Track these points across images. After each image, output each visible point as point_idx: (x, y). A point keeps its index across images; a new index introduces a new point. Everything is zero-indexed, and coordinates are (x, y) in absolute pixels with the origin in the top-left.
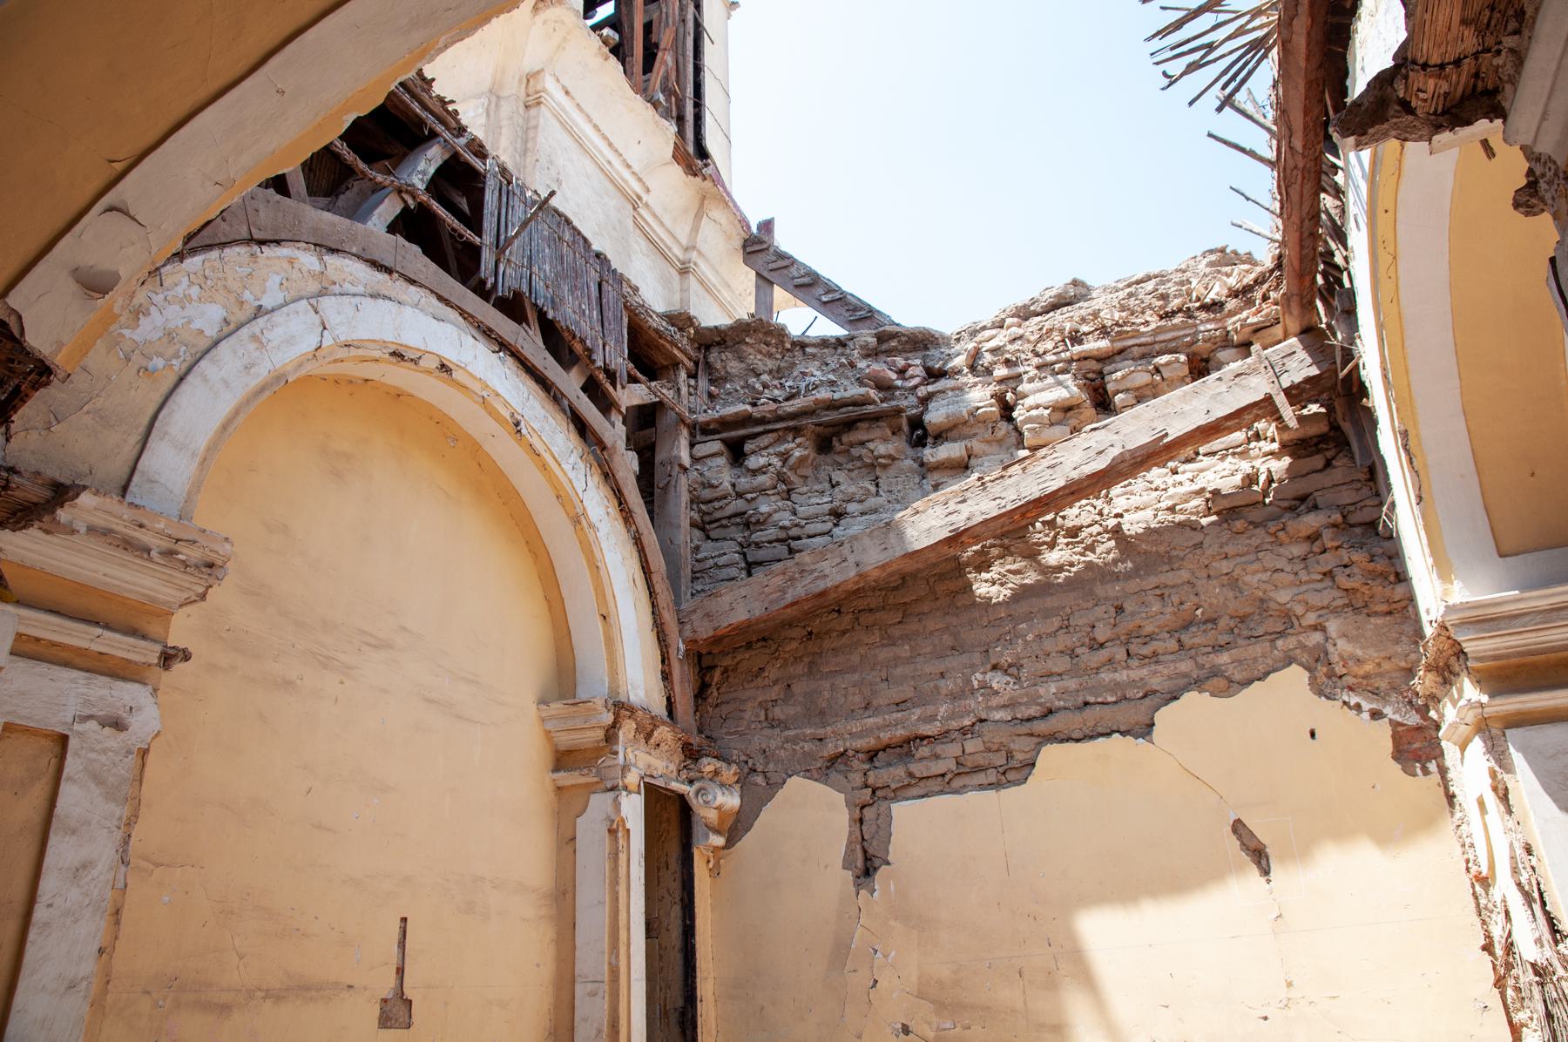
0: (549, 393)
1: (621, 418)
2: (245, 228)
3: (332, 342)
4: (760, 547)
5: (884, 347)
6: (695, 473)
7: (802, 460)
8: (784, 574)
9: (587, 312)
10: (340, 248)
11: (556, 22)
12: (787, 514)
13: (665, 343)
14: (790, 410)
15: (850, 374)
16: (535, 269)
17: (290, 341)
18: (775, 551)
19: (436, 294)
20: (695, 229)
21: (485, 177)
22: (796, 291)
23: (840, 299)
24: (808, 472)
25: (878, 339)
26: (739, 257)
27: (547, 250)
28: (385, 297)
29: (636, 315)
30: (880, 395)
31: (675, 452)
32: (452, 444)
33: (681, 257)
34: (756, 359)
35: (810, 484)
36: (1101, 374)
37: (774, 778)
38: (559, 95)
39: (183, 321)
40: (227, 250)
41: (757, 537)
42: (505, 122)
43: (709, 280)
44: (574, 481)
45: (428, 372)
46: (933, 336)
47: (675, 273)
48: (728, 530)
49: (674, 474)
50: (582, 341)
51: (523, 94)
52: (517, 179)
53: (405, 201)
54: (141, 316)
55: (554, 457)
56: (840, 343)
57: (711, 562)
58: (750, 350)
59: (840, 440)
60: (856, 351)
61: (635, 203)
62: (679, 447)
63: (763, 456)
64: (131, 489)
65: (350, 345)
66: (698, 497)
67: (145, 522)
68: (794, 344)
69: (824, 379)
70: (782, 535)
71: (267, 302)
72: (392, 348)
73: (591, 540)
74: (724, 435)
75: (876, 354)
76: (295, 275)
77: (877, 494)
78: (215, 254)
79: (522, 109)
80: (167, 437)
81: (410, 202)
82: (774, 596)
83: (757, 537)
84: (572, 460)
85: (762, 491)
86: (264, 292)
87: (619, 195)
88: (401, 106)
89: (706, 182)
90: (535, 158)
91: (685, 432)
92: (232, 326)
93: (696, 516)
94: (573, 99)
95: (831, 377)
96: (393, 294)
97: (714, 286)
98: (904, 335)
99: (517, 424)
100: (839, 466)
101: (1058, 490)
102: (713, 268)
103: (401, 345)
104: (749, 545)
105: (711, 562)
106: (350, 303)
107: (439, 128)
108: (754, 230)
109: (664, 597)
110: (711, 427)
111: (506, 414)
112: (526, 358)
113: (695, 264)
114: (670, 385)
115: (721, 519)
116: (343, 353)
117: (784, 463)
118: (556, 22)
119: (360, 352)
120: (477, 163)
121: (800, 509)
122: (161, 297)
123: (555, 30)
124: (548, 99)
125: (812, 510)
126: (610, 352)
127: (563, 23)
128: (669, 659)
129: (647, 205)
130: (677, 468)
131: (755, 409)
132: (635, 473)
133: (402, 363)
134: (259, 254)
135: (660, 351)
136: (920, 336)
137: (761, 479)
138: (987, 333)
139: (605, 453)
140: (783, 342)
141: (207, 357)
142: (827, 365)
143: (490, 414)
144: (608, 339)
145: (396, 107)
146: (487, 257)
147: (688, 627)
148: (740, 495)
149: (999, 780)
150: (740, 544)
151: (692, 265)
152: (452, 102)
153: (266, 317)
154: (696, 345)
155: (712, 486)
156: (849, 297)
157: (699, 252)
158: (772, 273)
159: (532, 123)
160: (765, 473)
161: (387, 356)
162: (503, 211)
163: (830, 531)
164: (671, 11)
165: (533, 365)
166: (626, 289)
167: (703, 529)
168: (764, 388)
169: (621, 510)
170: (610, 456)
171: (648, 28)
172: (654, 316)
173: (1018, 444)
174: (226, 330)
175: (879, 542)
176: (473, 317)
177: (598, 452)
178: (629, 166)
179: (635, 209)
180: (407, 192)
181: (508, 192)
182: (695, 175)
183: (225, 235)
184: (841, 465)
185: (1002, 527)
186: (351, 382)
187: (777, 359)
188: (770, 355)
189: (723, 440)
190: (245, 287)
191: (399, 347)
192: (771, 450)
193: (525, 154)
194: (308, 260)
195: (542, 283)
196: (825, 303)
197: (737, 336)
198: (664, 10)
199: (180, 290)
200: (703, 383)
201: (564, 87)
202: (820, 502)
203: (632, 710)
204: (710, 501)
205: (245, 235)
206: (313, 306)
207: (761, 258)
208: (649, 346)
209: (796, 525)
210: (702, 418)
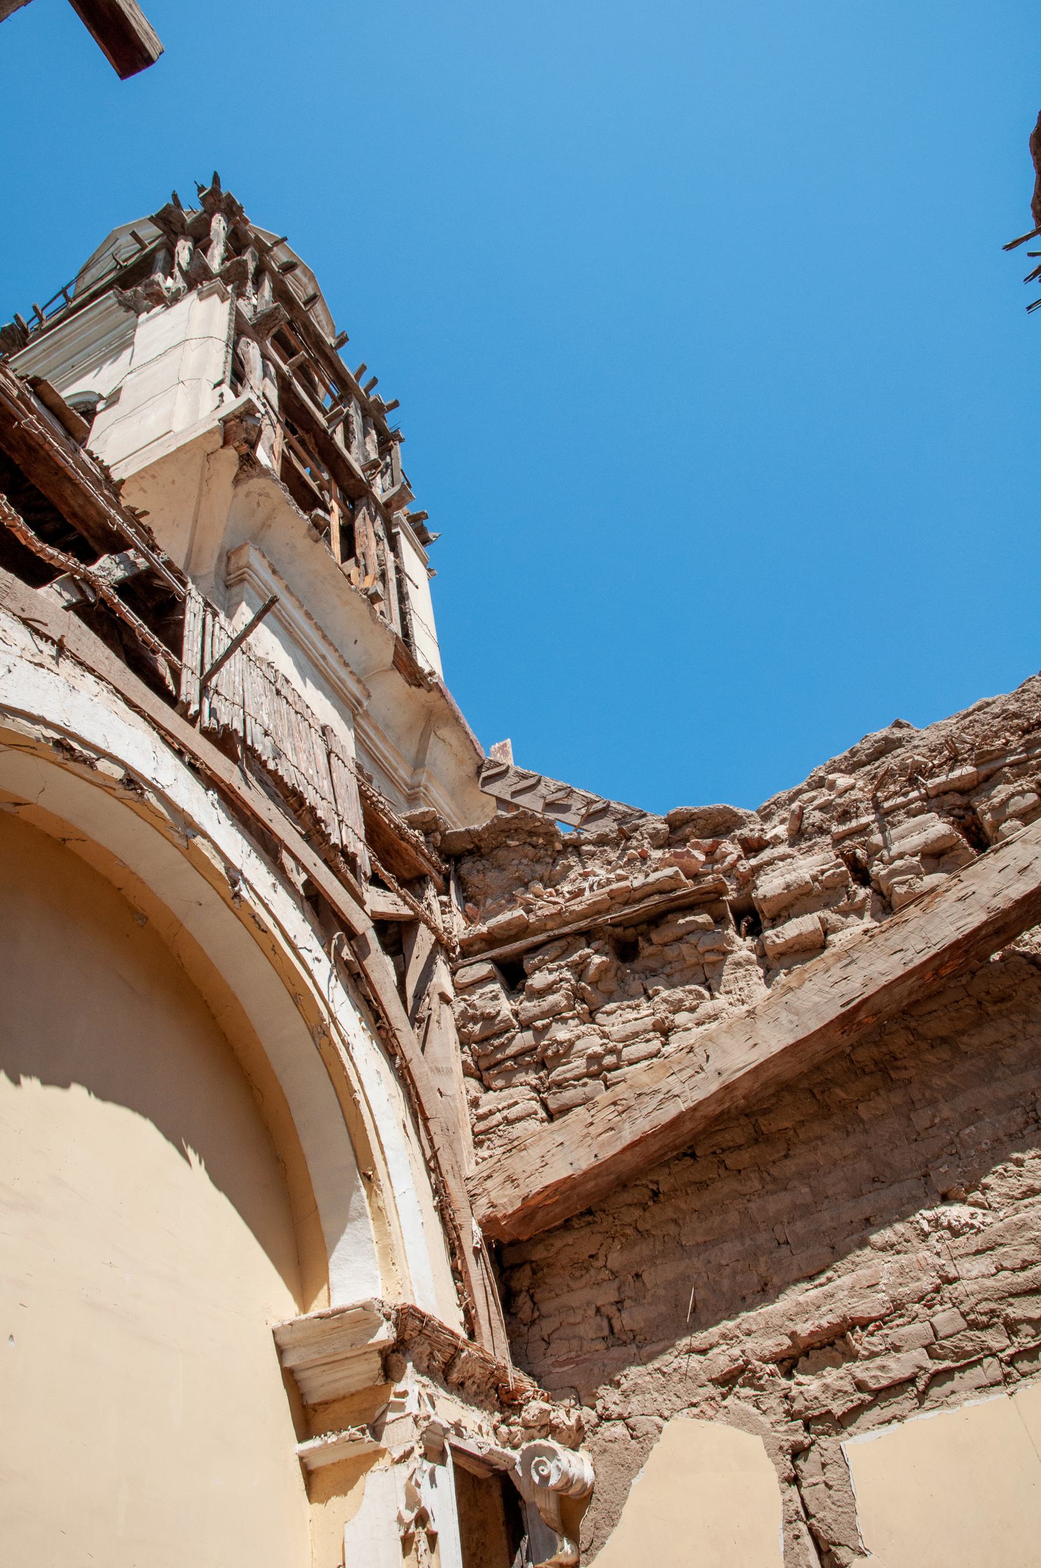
7: (602, 969)
11: (260, 495)
12: (597, 1040)
18: (586, 1089)
33: (409, 781)
36: (970, 808)
37: (644, 1425)
38: (266, 574)
57: (498, 1117)
77: (713, 997)
101: (979, 929)
105: (498, 1117)
124: (250, 572)
127: (268, 496)
129: (366, 715)
137: (551, 999)
138: (805, 796)
147: (483, 1201)
149: (1007, 1375)
150: (535, 1089)
152: (145, 513)
163: (659, 1051)
167: (480, 1079)
169: (379, 1028)
173: (884, 908)
175: (744, 1038)
178: (346, 665)
182: (419, 686)
185: (910, 994)
189: (494, 960)
202: (639, 1016)
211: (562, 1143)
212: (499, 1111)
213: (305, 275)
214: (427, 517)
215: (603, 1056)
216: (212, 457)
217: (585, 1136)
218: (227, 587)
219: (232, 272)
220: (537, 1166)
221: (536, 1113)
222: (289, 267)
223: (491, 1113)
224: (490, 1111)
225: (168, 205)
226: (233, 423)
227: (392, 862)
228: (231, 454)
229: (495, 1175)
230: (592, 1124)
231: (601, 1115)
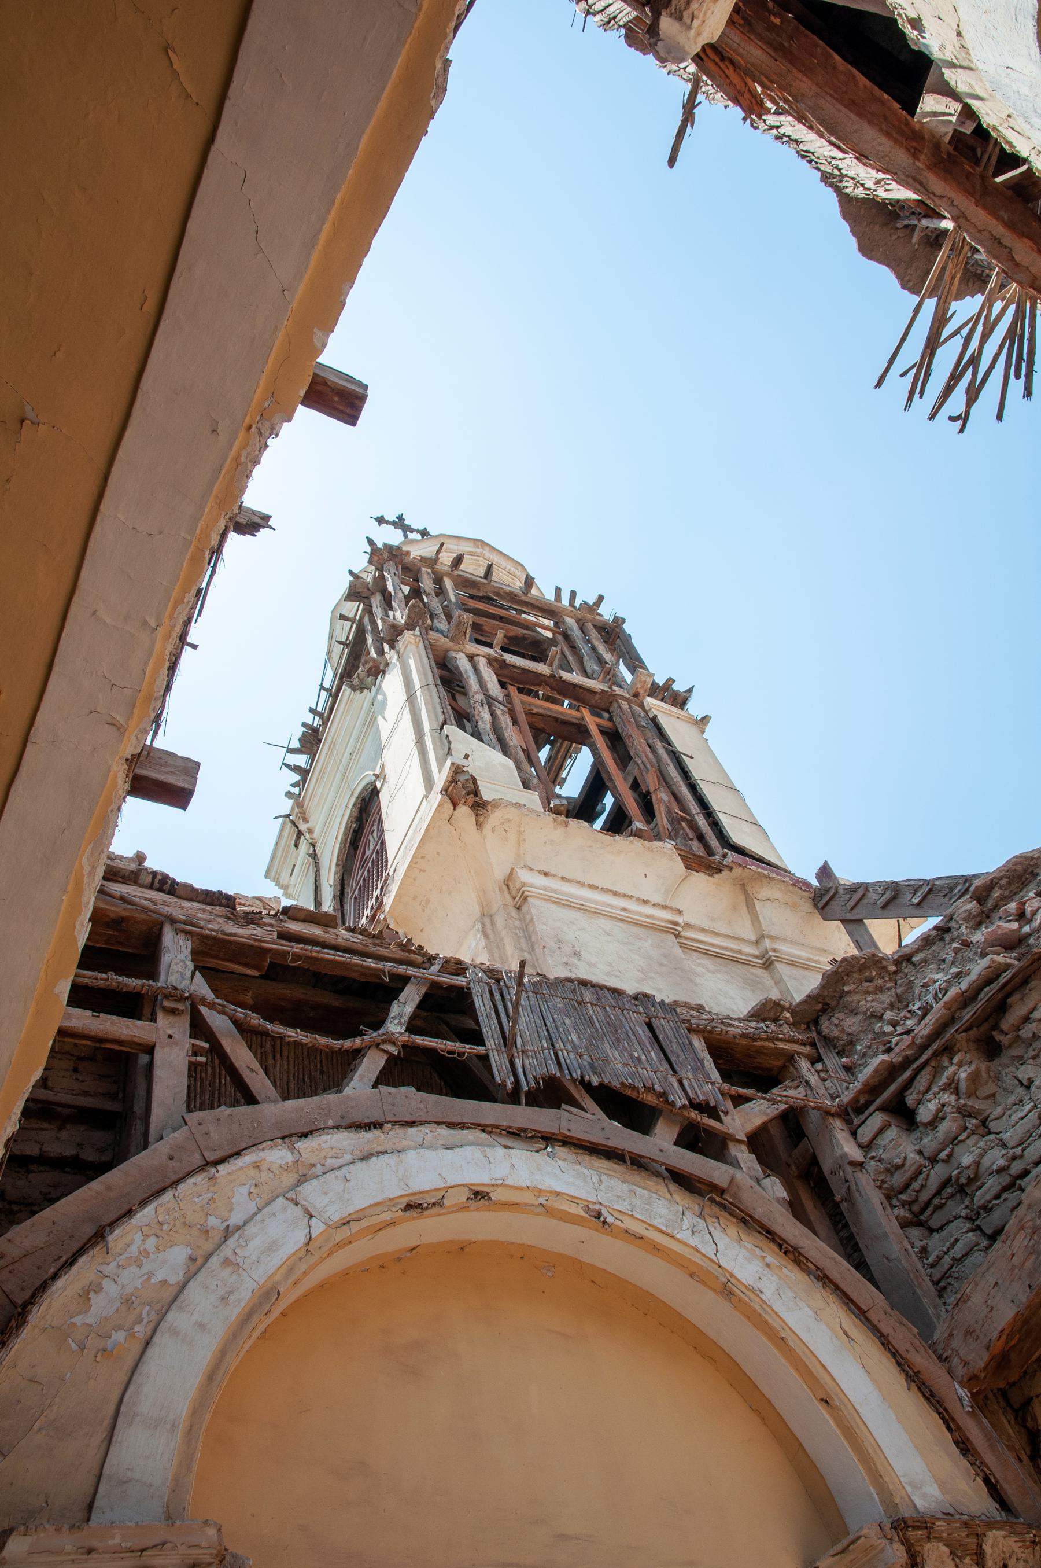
0: (624, 1161)
1: (744, 1148)
2: (197, 1156)
3: (323, 1227)
4: (991, 1209)
5: (990, 904)
6: (873, 1163)
7: (974, 1079)
8: (1022, 1228)
9: (643, 1057)
10: (314, 1128)
11: (502, 824)
13: (763, 1043)
14: (925, 1032)
15: (971, 955)
16: (559, 1045)
17: (272, 1247)
19: (444, 1123)
20: (755, 918)
21: (469, 988)
22: (887, 912)
23: (930, 890)
24: (990, 1088)
25: (979, 902)
26: (817, 915)
27: (567, 1021)
28: (379, 1153)
29: (711, 1032)
30: (1014, 954)
31: (838, 1152)
32: (550, 1274)
33: (757, 953)
34: (868, 1003)
35: (1002, 1101)
38: (540, 881)
39: (140, 1280)
40: (182, 1187)
41: (981, 1197)
42: (504, 933)
43: (799, 957)
44: (700, 1247)
45: (463, 1208)
46: (1032, 858)
47: (759, 971)
48: (946, 1208)
49: (849, 1177)
50: (649, 1089)
51: (509, 900)
52: (506, 973)
53: (386, 1052)
54: (92, 1295)
55: (662, 1232)
56: (942, 931)
57: (947, 1259)
58: (857, 997)
59: (1002, 1031)
60: (963, 927)
61: (674, 931)
62: (839, 1144)
63: (930, 1100)
64: (97, 1503)
65: (348, 1222)
66: (892, 1188)
67: (95, 1544)
68: (897, 962)
69: (949, 976)
70: (1005, 1180)
71: (236, 1219)
72: (404, 1202)
73: (757, 1307)
74: (878, 1102)
75: (988, 917)
76: (264, 1176)
78: (168, 1196)
79: (514, 913)
80: (137, 1419)
81: (392, 1049)
82: (1029, 1264)
83: (981, 1197)
84: (686, 1224)
85: (954, 1140)
86: (232, 1210)
87: (651, 932)
88: (367, 971)
89: (733, 871)
90: (541, 947)
91: (838, 1123)
92: (200, 1261)
93: (902, 1212)
94: (554, 876)
95: (954, 970)
96: (388, 1146)
97: (809, 959)
98: (1001, 878)
99: (598, 1215)
100: (1021, 1060)
102: (794, 943)
103: (414, 1194)
104: (978, 1214)
105: (947, 1259)
106: (336, 1177)
107: (402, 969)
108: (815, 883)
109: (903, 1336)
110: (862, 1101)
111: (578, 1211)
112: (579, 1139)
113: (774, 951)
114: (795, 1083)
115: (931, 1199)
116: (345, 1233)
117: (957, 1094)
118: (502, 824)
119: (365, 1223)
120: (459, 981)
121: (1005, 1136)
122: (113, 1265)
123: (506, 831)
125: (1020, 1130)
126: (691, 1085)
127: (509, 821)
128: (953, 1419)
129: (688, 926)
130: (849, 1169)
131: (892, 1054)
132: (780, 1201)
133: (426, 1213)
134: (217, 1175)
135: (763, 1053)
136: (1018, 868)
137: (944, 1127)
139: (726, 1196)
140: (884, 968)
141: (174, 1307)
142: (944, 961)
143: (561, 1220)
144: (682, 1073)
145: (363, 974)
146: (498, 1062)
147: (956, 1361)
148: (933, 1160)
150: (967, 1218)
151: (771, 953)
153: (237, 1235)
154: (803, 1026)
155: (898, 1167)
156: (937, 882)
157: (771, 937)
158: (855, 911)
159: (528, 918)
160: (943, 1118)
161: (400, 1213)
162: (501, 1008)
164: (645, 758)
165: (591, 1143)
166: (686, 1014)
167: (920, 1224)
168: (894, 1026)
169: (785, 1253)
170: (735, 1196)
171: (635, 786)
172: (736, 1023)
174: (193, 1269)
176: (497, 1127)
177: (718, 1199)
178: (645, 902)
179: (677, 936)
180: (384, 1042)
181: (501, 989)
182: (720, 871)
183: (175, 1172)
184: (1021, 1057)
186: (399, 1259)
187: (889, 989)
188: (880, 989)
189: (881, 1109)
190: (207, 1214)
191: (412, 1198)
192: (935, 1089)
193: (533, 950)
194: (278, 1156)
195: (572, 1056)
196: (919, 904)
197: (835, 991)
198: (640, 762)
199: (134, 1249)
200: (832, 1061)
201: (539, 871)
202: (1022, 1114)
203: (925, 1524)
204: (907, 1186)
205: (197, 1160)
206: (291, 1200)
207: (836, 905)
208: (750, 1056)
209: (1014, 1158)
210: (846, 1097)
211: (997, 1283)
212: (946, 1253)
213: (477, 547)
214: (674, 681)
215: (1009, 1166)
216: (452, 819)
217: (1012, 1270)
218: (519, 908)
219: (413, 615)
220: (985, 1312)
221: (977, 1244)
222: (458, 560)
223: (939, 1258)
224: (938, 1257)
225: (351, 583)
226: (451, 788)
227: (758, 1060)
228: (464, 810)
229: (955, 1332)
230: (1013, 1255)
231: (1016, 1243)
